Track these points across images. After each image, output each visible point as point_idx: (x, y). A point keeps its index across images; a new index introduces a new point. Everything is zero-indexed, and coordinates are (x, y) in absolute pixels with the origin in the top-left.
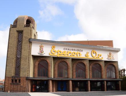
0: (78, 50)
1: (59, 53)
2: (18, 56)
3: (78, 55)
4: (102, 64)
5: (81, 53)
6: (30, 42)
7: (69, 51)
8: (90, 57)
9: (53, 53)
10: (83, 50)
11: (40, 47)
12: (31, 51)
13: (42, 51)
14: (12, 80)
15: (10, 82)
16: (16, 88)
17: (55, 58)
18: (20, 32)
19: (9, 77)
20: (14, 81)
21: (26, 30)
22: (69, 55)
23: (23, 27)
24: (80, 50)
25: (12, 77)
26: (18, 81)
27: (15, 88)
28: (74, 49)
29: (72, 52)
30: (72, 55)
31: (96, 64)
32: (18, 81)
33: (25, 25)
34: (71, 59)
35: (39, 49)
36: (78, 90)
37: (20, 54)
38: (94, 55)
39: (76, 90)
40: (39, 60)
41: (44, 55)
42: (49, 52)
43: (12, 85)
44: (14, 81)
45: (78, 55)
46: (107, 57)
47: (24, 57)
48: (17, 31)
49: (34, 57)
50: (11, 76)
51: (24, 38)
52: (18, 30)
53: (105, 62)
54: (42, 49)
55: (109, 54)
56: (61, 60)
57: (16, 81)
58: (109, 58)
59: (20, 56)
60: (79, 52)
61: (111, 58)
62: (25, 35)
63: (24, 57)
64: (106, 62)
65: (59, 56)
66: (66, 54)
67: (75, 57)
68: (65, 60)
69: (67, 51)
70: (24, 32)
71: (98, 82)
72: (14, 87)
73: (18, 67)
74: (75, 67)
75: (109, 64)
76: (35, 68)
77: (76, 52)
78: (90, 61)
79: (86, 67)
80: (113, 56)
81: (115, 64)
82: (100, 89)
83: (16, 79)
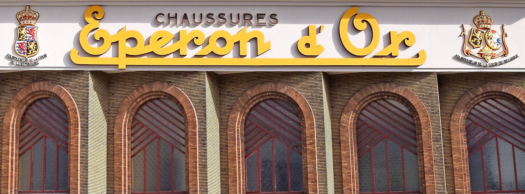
0: (247, 17)
1: (126, 47)
3: (247, 48)
4: (425, 100)
5: (267, 34)
7: (188, 31)
8: (328, 54)
9: (93, 48)
10: (280, 13)
11: (19, 20)
13: (26, 45)
17: (108, 80)
22: (190, 53)
24: (260, 16)
28: (221, 16)
29: (209, 31)
30: (207, 50)
31: (383, 96)
38: (356, 42)
40: (20, 97)
41: (43, 65)
42: (69, 46)
45: (247, 48)
53: (445, 79)
54: (31, 32)
56: (375, 89)
58: (475, 52)
60: (250, 31)
61: (487, 50)
65: (122, 64)
67: (228, 60)
68: (399, 84)
69: (172, 30)
74: (238, 127)
75: (480, 91)
77: (232, 32)
78: (335, 81)
80: (504, 35)
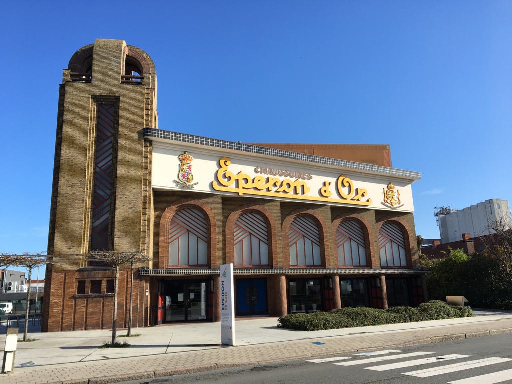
2: (100, 192)
6: (145, 136)
9: (224, 181)
12: (151, 172)
14: (79, 282)
15: (73, 290)
16: (97, 313)
18: (108, 108)
19: (65, 273)
20: (89, 288)
21: (128, 97)
23: (117, 82)
25: (79, 271)
26: (104, 285)
27: (92, 313)
30: (282, 190)
31: (252, 212)
32: (104, 285)
33: (123, 78)
34: (279, 205)
35: (192, 171)
36: (305, 311)
37: (109, 186)
39: (189, 318)
41: (196, 189)
43: (79, 301)
44: (89, 288)
45: (299, 190)
46: (381, 198)
47: (127, 193)
48: (95, 98)
49: (163, 198)
50: (76, 268)
51: (123, 127)
52: (97, 93)
54: (190, 168)
55: (386, 189)
57: (97, 285)
59: (108, 192)
62: (125, 114)
63: (127, 193)
64: (380, 215)
66: (262, 185)
70: (123, 102)
71: (202, 282)
72: (90, 310)
73: (103, 236)
76: (162, 234)
79: (324, 230)
81: (403, 221)
82: (18, 330)
83: (99, 275)
